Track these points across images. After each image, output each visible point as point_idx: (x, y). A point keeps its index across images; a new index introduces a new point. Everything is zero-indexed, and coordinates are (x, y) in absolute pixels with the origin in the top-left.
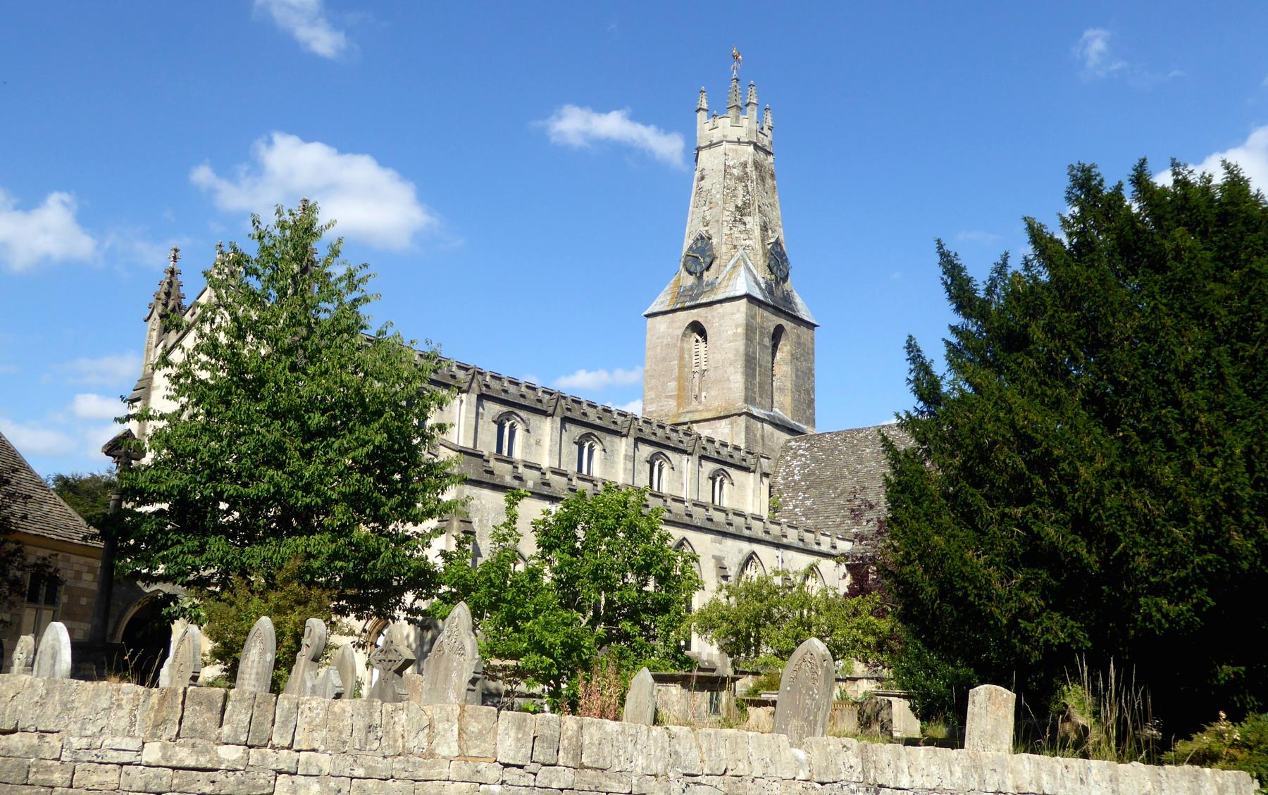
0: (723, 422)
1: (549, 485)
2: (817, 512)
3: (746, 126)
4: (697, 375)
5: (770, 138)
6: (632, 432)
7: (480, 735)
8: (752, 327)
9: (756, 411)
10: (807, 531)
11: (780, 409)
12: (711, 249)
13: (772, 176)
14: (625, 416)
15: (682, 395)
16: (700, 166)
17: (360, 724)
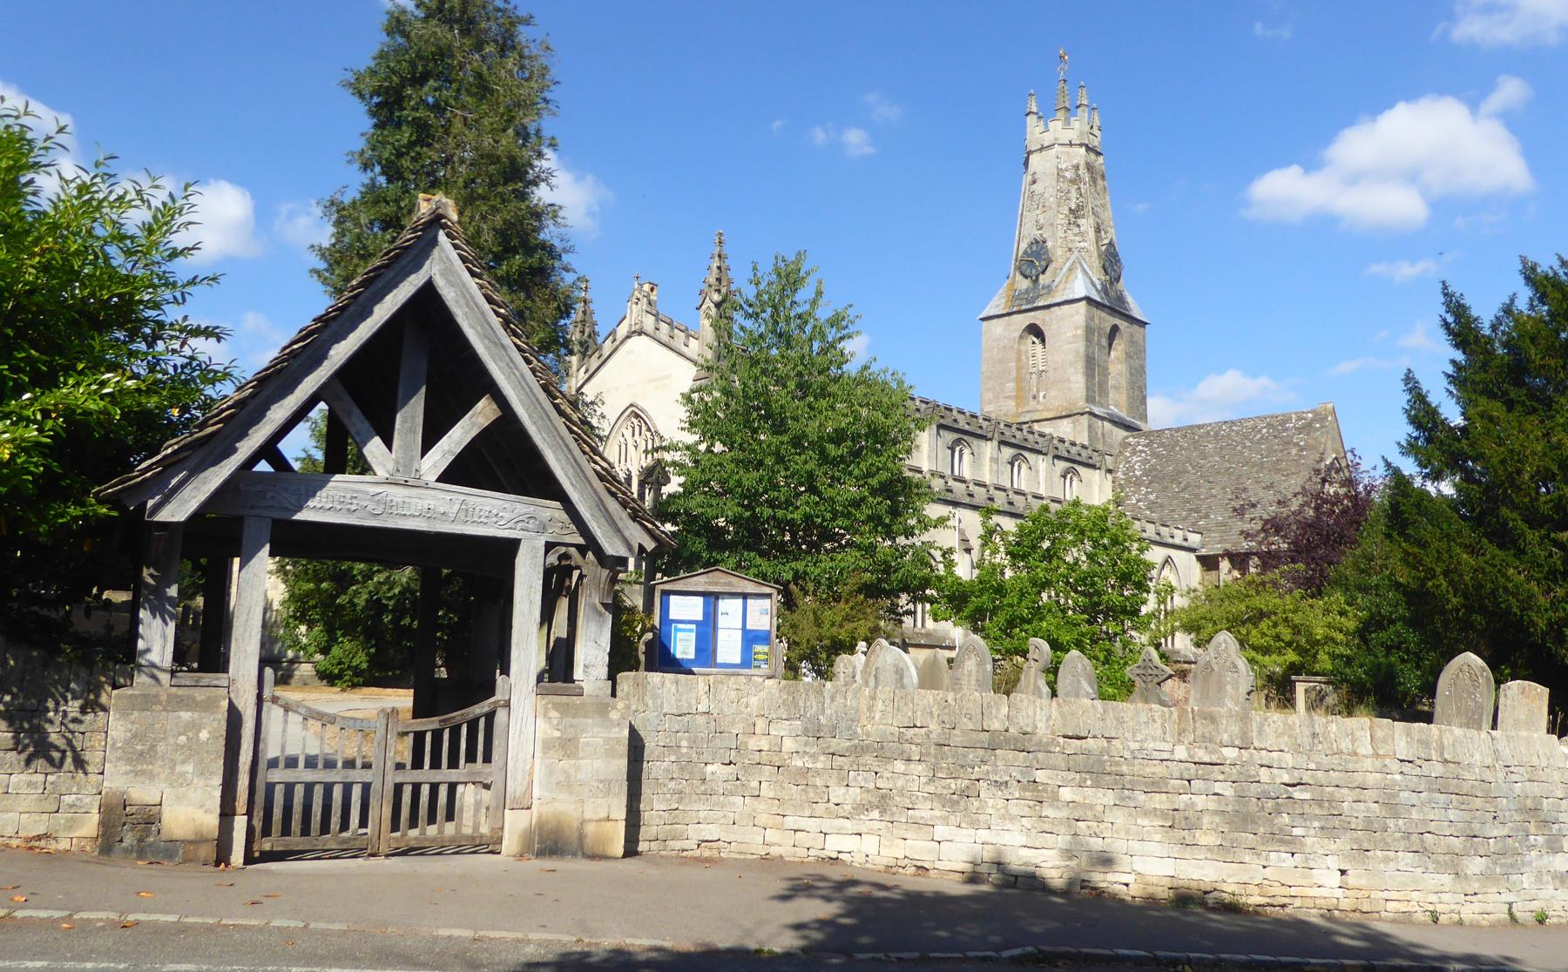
0: (1065, 421)
1: (951, 491)
2: (1161, 506)
3: (1078, 127)
4: (1034, 376)
6: (996, 436)
7: (1384, 740)
9: (1097, 410)
10: (1163, 525)
11: (1116, 406)
12: (1047, 252)
13: (1103, 177)
14: (989, 421)
15: (1020, 397)
16: (1031, 169)
17: (1307, 732)
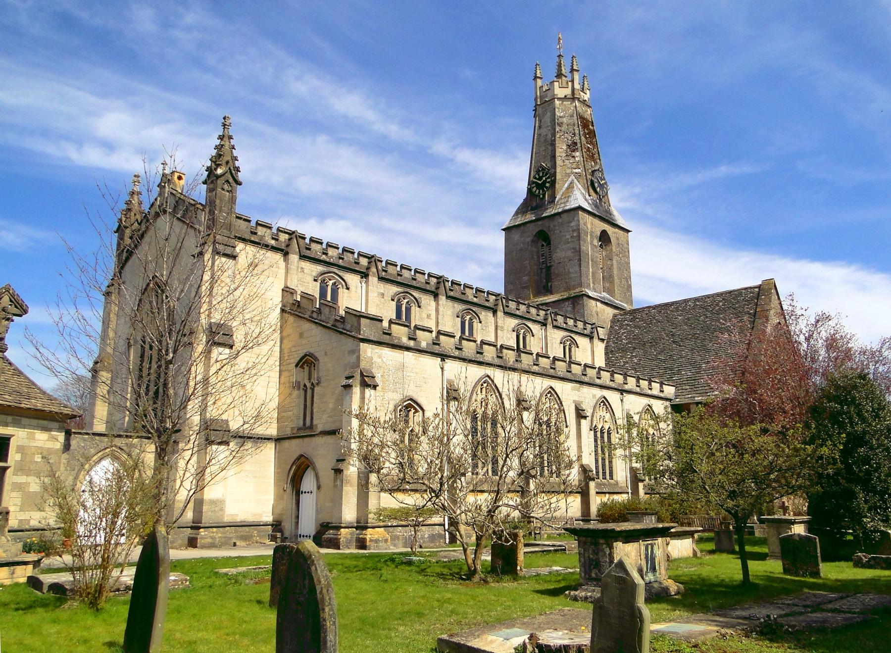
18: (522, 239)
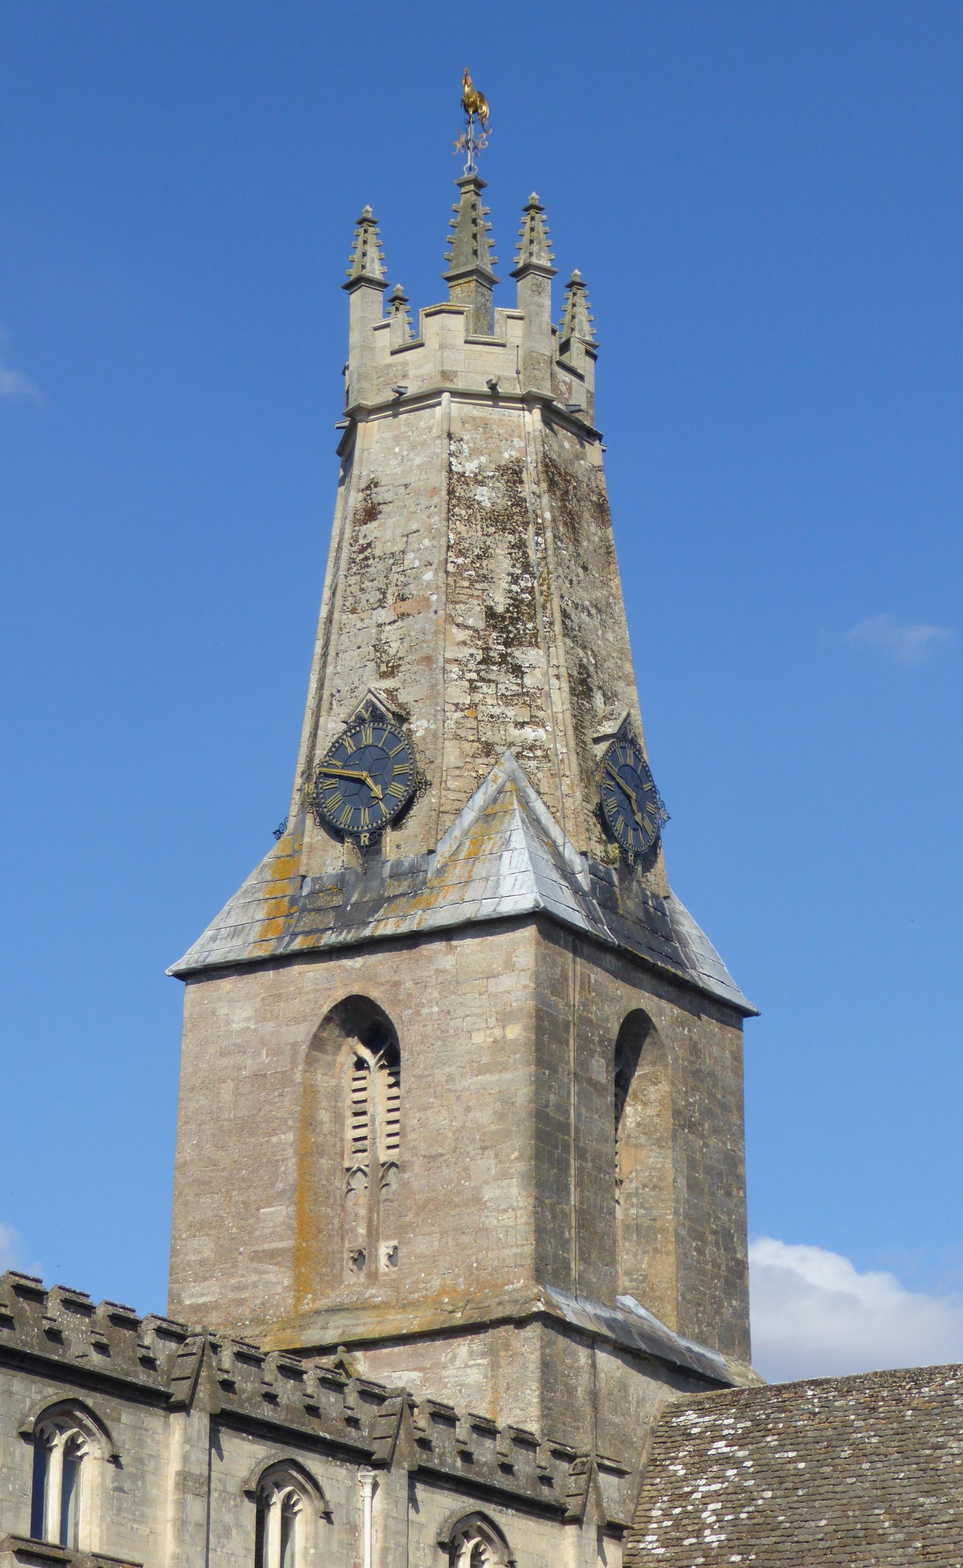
0: (462, 1347)
5: (589, 383)
6: (203, 1393)
8: (553, 1020)
11: (641, 1297)
12: (408, 754)
13: (601, 510)
14: (180, 1338)
16: (361, 471)
18: (270, 1026)
